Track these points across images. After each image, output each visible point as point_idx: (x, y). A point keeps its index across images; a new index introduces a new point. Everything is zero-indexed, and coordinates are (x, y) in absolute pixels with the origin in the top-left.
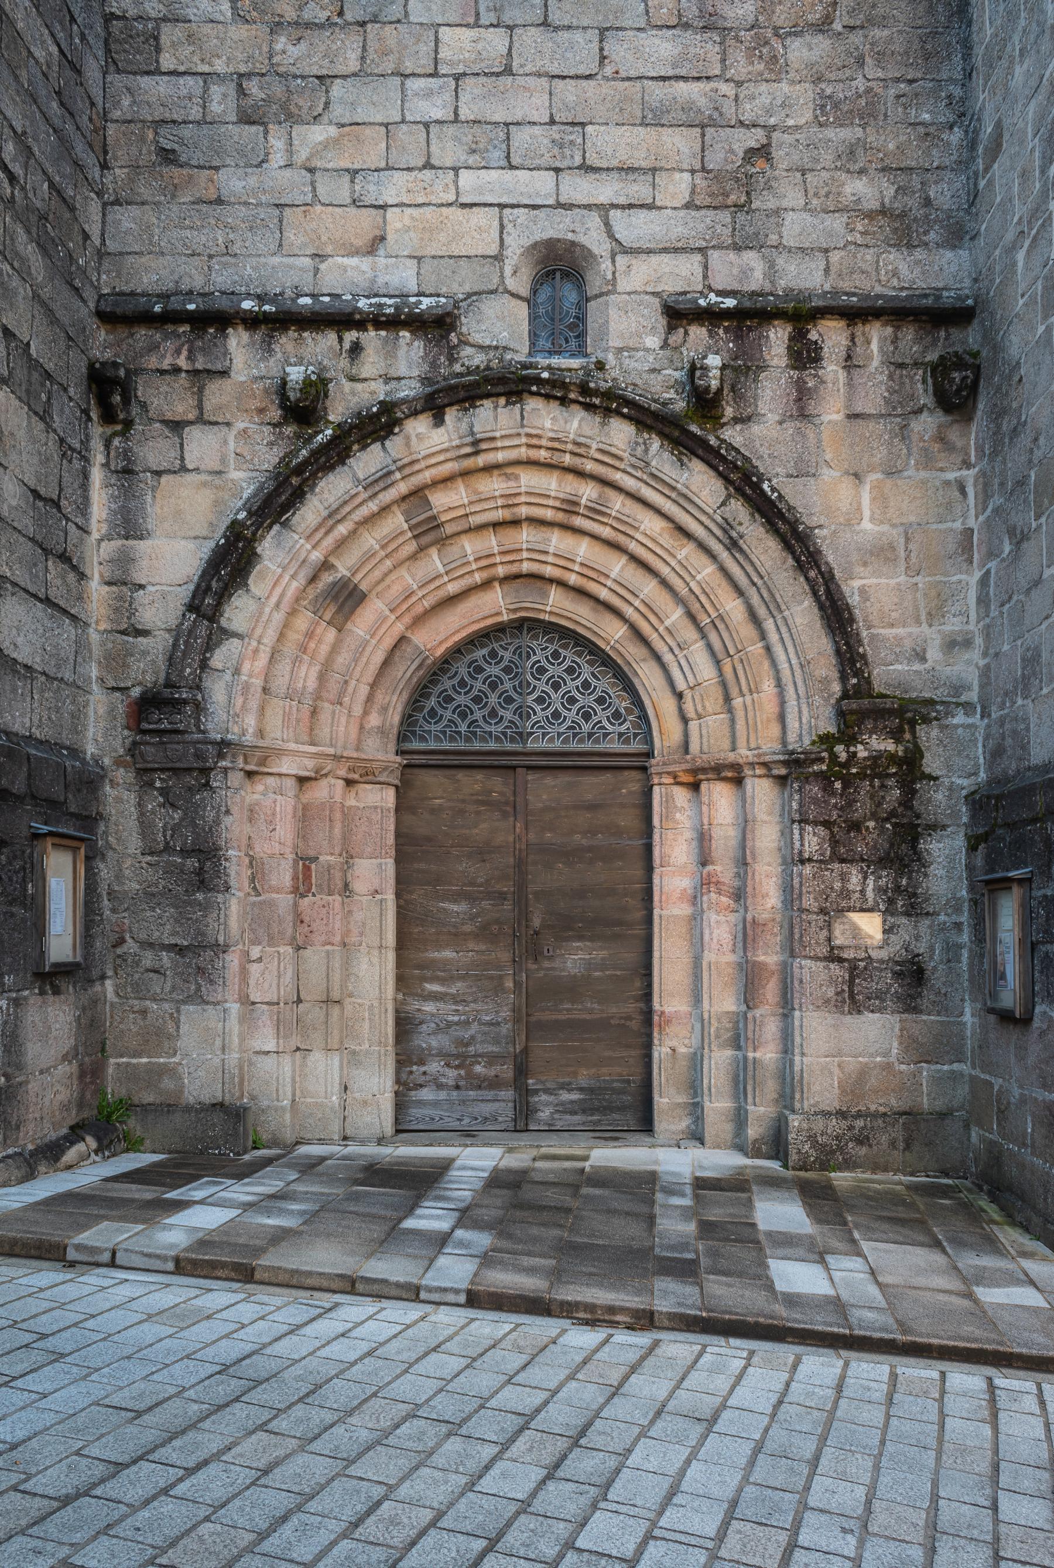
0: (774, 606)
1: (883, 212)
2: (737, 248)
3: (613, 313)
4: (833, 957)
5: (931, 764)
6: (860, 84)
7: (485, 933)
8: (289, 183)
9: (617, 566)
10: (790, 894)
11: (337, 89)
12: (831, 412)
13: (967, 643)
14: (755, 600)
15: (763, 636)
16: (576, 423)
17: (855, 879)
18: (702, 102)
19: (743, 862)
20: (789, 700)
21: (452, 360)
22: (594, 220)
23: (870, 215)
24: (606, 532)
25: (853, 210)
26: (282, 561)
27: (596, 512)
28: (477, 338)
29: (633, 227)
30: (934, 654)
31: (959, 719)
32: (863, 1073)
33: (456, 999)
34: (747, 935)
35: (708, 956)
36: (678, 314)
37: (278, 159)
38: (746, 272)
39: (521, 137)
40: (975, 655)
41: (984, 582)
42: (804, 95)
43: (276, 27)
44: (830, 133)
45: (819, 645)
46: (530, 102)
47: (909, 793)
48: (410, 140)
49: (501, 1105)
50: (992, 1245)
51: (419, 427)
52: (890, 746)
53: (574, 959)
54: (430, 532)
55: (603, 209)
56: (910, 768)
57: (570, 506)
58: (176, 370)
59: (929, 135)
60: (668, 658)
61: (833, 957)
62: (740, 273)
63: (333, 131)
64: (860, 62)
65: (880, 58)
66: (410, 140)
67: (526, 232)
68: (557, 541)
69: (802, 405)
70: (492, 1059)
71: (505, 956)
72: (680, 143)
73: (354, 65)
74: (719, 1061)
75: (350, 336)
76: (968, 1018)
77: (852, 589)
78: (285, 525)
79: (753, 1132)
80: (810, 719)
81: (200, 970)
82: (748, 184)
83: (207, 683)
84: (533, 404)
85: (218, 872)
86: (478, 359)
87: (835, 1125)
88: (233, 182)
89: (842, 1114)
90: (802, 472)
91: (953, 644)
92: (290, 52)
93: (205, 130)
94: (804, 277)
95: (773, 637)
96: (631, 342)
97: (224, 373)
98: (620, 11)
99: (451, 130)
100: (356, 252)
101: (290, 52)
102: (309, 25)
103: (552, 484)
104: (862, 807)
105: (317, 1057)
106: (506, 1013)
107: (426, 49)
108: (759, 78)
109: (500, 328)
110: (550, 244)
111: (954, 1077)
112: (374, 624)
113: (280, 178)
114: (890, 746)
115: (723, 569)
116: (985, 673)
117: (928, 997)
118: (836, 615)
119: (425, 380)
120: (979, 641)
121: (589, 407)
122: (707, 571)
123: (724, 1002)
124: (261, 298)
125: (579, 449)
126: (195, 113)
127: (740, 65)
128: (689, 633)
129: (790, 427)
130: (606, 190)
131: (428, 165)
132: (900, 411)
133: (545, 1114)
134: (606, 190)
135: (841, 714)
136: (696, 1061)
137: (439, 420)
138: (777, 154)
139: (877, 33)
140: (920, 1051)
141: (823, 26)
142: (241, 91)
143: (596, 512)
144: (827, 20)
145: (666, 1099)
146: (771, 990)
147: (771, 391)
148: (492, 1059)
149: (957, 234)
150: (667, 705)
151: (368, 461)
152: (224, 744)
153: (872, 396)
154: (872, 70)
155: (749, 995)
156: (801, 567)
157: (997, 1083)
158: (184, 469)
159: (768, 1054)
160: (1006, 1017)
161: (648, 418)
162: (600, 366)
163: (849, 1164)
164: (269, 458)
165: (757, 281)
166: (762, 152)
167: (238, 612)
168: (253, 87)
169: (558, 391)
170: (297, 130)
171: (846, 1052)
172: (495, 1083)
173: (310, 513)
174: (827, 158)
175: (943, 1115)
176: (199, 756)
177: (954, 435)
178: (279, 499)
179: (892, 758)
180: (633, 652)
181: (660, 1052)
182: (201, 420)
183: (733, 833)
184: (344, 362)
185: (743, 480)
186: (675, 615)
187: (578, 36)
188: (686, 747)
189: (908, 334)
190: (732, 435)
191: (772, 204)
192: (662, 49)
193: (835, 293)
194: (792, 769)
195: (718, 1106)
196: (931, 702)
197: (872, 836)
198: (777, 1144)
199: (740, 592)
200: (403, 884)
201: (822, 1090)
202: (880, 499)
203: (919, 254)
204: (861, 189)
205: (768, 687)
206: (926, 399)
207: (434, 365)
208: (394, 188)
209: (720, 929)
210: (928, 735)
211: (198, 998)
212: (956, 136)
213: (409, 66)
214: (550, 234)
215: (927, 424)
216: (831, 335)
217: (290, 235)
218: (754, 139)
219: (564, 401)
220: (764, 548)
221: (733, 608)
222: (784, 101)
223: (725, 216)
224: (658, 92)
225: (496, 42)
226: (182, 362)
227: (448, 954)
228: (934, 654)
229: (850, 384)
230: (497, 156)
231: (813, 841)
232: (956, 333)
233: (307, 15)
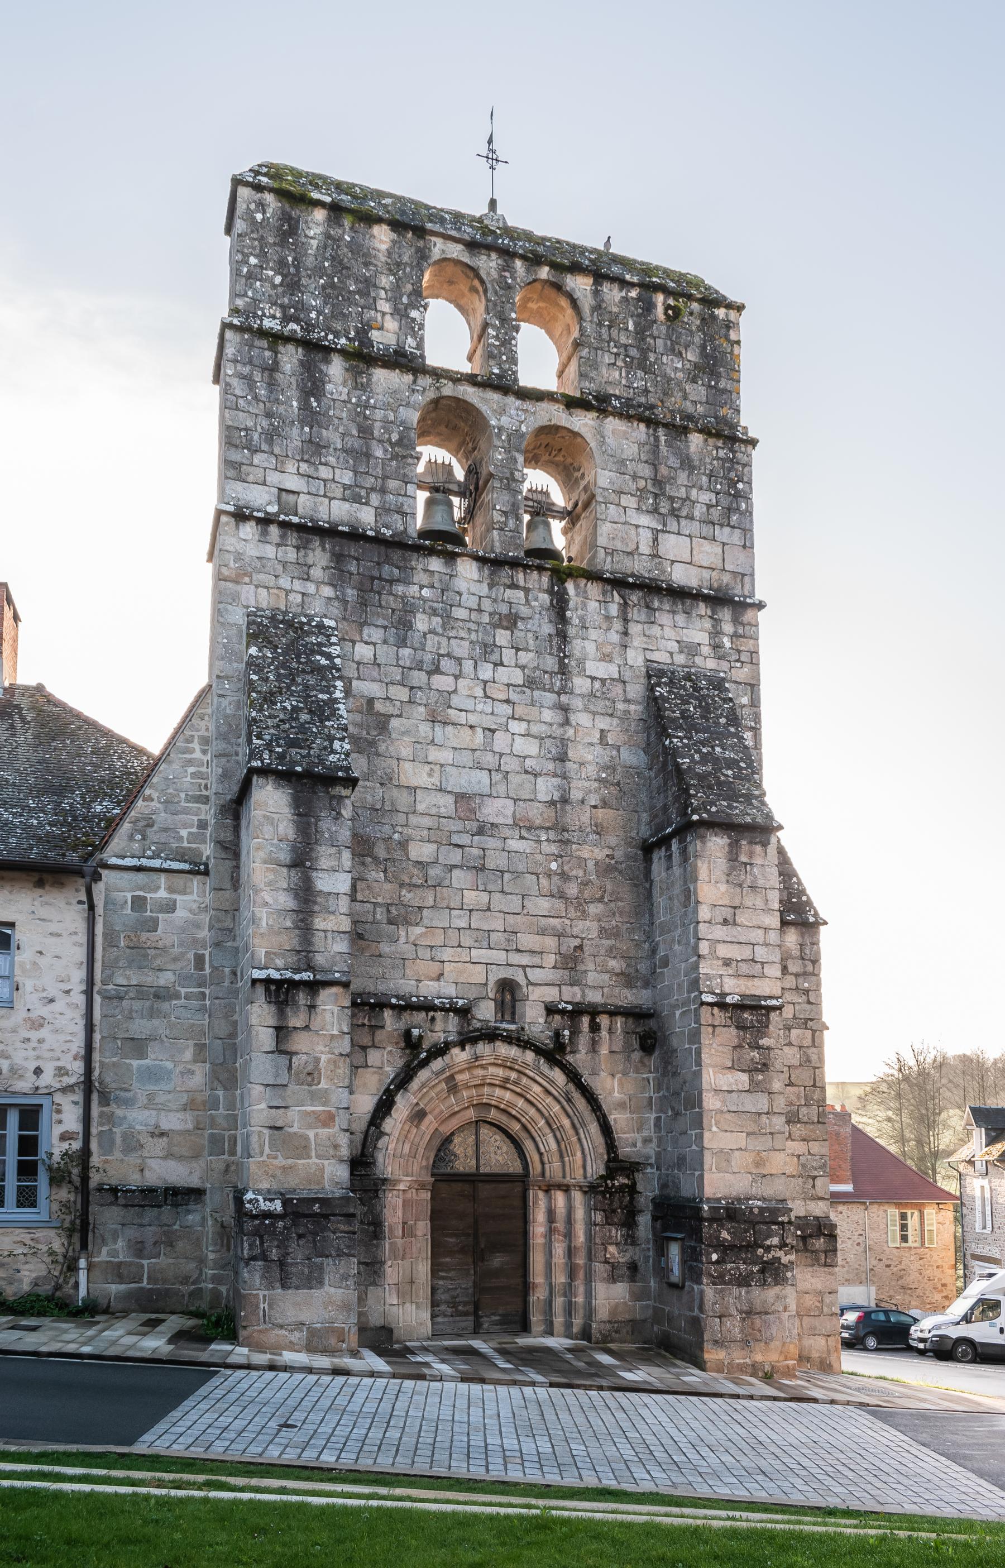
0: (583, 1125)
1: (622, 973)
2: (571, 985)
3: (527, 1009)
4: (606, 1262)
5: (640, 1187)
6: (614, 923)
7: (462, 1251)
8: (408, 950)
9: (520, 1103)
10: (590, 1237)
11: (425, 912)
12: (604, 1051)
13: (651, 1141)
14: (576, 1121)
15: (577, 1134)
16: (513, 1052)
17: (614, 1231)
18: (559, 927)
19: (569, 1221)
20: (587, 1161)
21: (469, 1025)
22: (520, 971)
23: (617, 975)
24: (518, 1090)
25: (612, 972)
26: (403, 1106)
27: (516, 1083)
28: (479, 1017)
29: (535, 975)
30: (639, 1144)
31: (649, 1170)
32: (617, 1305)
33: (451, 1279)
34: (570, 1252)
35: (554, 1260)
36: (551, 1010)
37: (403, 940)
38: (574, 995)
39: (494, 936)
40: (654, 1145)
41: (658, 1119)
42: (594, 926)
43: (402, 885)
44: (604, 941)
45: (599, 1140)
46: (497, 923)
47: (632, 1199)
48: (453, 934)
49: (469, 1322)
50: (675, 1366)
51: (455, 1051)
52: (626, 1181)
53: (497, 1261)
54: (453, 1088)
55: (524, 967)
56: (632, 1190)
57: (507, 1080)
58: (364, 1025)
59: (638, 945)
60: (538, 1139)
61: (606, 1262)
62: (572, 994)
63: (424, 930)
64: (614, 914)
65: (621, 913)
66: (453, 934)
67: (497, 974)
68: (498, 1092)
69: (594, 1047)
70: (465, 1304)
71: (471, 1260)
72: (551, 942)
73: (431, 903)
74: (559, 1302)
75: (431, 1014)
76: (652, 1283)
77: (611, 1118)
78: (406, 1089)
79: (575, 1330)
80: (596, 1168)
81: (375, 1272)
82: (575, 960)
83: (376, 1154)
84: (498, 1043)
85: (382, 1232)
86: (478, 1025)
87: (608, 1326)
88: (385, 948)
89: (610, 1322)
90: (594, 1073)
91: (647, 1141)
92: (407, 896)
93: (375, 926)
94: (595, 997)
95: (582, 1136)
96: (534, 1019)
97: (383, 1027)
98: (529, 889)
99: (468, 932)
100: (432, 980)
101: (407, 896)
102: (415, 886)
103: (500, 1072)
104: (616, 1205)
105: (408, 1305)
106: (471, 1284)
107: (458, 898)
108: (579, 919)
109: (486, 1012)
110: (505, 979)
111: (648, 1306)
112: (429, 1124)
113: (403, 947)
114: (626, 1181)
115: (563, 1108)
116: (658, 1154)
117: (639, 1276)
118: (606, 1129)
119: (460, 1033)
120: (655, 1140)
121: (519, 1046)
122: (557, 1108)
123: (560, 1278)
124: (397, 997)
125: (514, 1061)
126: (370, 919)
127: (572, 914)
128: (547, 1130)
129: (590, 1056)
130: (525, 960)
131: (459, 946)
132: (627, 1049)
133: (486, 1326)
134: (525, 960)
135: (608, 1168)
136: (549, 1302)
137: (463, 1049)
138: (585, 949)
139: (620, 904)
140: (637, 1296)
141: (600, 900)
142: (388, 911)
143: (516, 1083)
144: (603, 897)
145: (536, 1318)
146: (581, 1274)
147: (583, 1041)
148: (465, 1304)
149: (646, 984)
150: (536, 1157)
151: (437, 1064)
152: (385, 1179)
153: (618, 1046)
154: (618, 919)
155: (572, 1275)
156: (594, 1110)
157: (667, 1309)
158: (367, 1066)
159: (580, 1299)
160: (673, 1286)
161: (539, 1051)
162: (523, 1029)
163: (613, 1341)
164: (400, 1063)
165: (578, 998)
166: (580, 948)
167: (388, 1125)
168: (393, 909)
169: (510, 1039)
170: (410, 928)
171: (610, 1297)
172: (466, 1314)
173: (415, 1084)
174: (603, 951)
175: (644, 1321)
176: (375, 1184)
177: (646, 1060)
178: (404, 1079)
179: (627, 1185)
180: (523, 1135)
181: (533, 1299)
182: (374, 1046)
183: (563, 1210)
184: (428, 1024)
185: (573, 1076)
186: (542, 1123)
187: (514, 897)
188: (543, 1174)
189: (630, 1021)
190: (570, 1058)
191: (583, 968)
192: (544, 905)
193: (606, 1005)
194: (591, 1190)
195: (559, 1320)
196: (638, 1163)
197: (619, 1215)
198: (586, 1334)
199: (569, 1116)
200: (433, 1230)
201: (603, 1313)
202: (621, 1084)
203: (634, 991)
204: (613, 964)
205: (579, 1154)
206: (636, 1046)
207: (462, 1027)
208: (447, 954)
209: (559, 1249)
210: (639, 1176)
211: (374, 1284)
212: (646, 946)
213: (452, 905)
214: (505, 976)
215: (637, 1055)
216: (604, 1020)
217: (407, 971)
218: (577, 942)
219: (510, 1043)
220: (581, 1103)
221: (566, 1122)
222: (587, 928)
223: (567, 972)
224: (543, 921)
225: (484, 897)
226: (366, 1022)
227: (448, 1260)
228: (639, 1144)
229: (610, 1039)
230: (485, 944)
231: (599, 1217)
232: (647, 1021)
233: (413, 881)
